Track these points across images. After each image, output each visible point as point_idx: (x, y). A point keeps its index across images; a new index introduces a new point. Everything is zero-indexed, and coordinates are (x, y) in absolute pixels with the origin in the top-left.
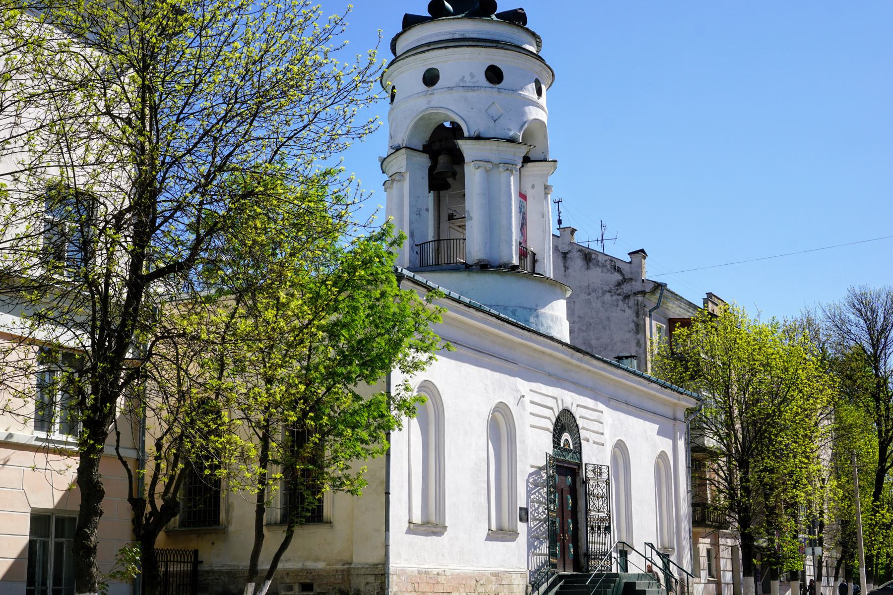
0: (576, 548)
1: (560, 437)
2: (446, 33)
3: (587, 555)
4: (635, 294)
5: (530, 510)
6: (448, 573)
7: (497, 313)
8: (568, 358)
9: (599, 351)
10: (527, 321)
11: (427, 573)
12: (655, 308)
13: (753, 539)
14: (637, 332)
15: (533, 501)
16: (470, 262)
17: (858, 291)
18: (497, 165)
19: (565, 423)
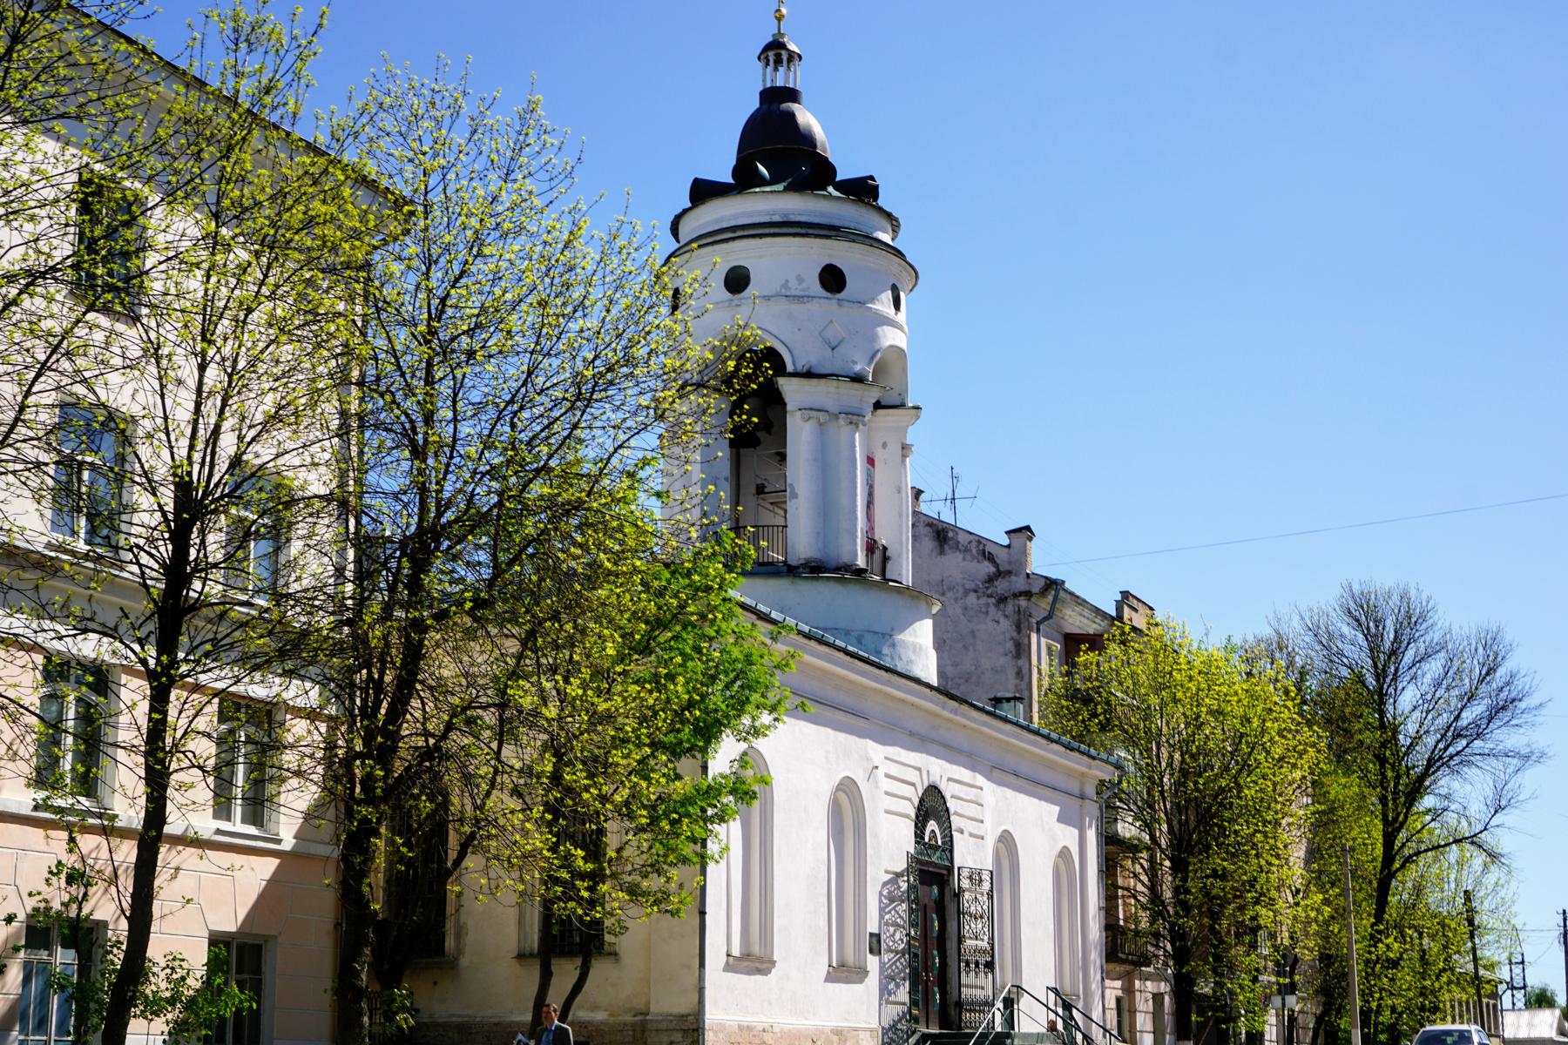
0: (943, 993)
1: (924, 827)
2: (759, 213)
3: (959, 1004)
4: (1015, 596)
5: (883, 937)
6: (776, 1030)
7: (843, 645)
8: (938, 709)
9: (975, 693)
10: (878, 653)
11: (749, 1028)
12: (1045, 619)
13: (1193, 983)
14: (1018, 656)
15: (887, 924)
16: (793, 561)
17: (1356, 589)
18: (836, 416)
19: (931, 807)
